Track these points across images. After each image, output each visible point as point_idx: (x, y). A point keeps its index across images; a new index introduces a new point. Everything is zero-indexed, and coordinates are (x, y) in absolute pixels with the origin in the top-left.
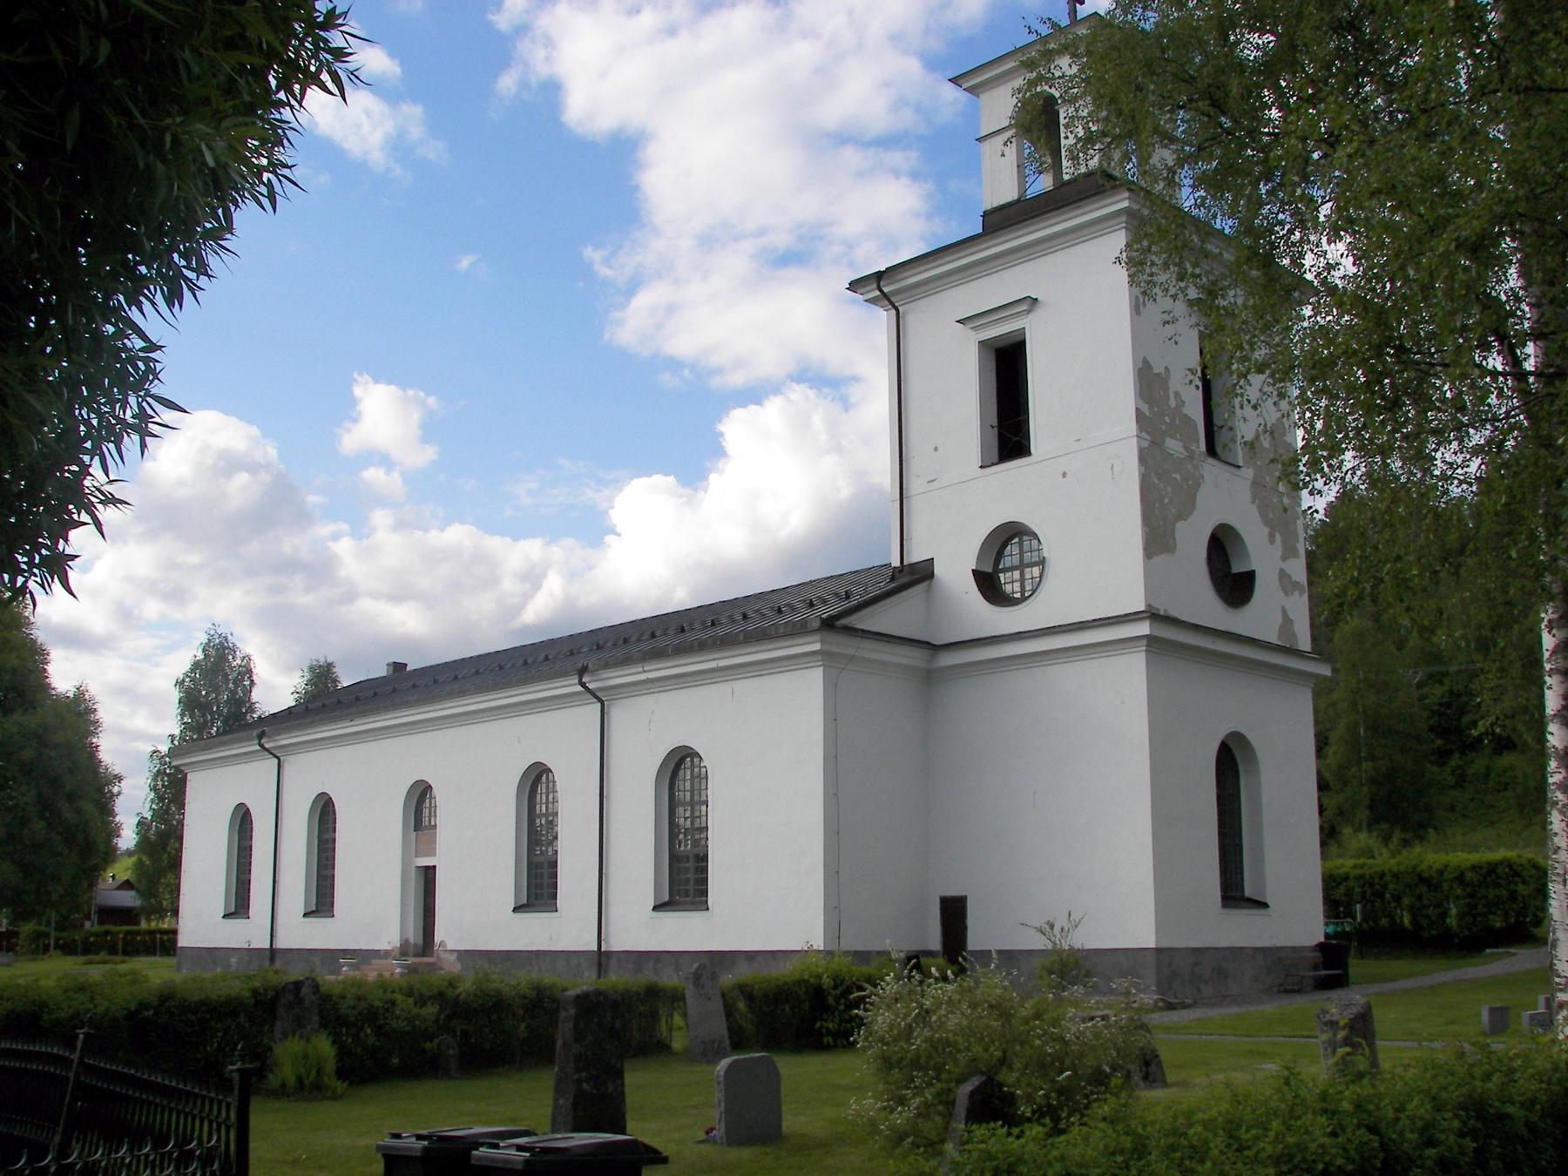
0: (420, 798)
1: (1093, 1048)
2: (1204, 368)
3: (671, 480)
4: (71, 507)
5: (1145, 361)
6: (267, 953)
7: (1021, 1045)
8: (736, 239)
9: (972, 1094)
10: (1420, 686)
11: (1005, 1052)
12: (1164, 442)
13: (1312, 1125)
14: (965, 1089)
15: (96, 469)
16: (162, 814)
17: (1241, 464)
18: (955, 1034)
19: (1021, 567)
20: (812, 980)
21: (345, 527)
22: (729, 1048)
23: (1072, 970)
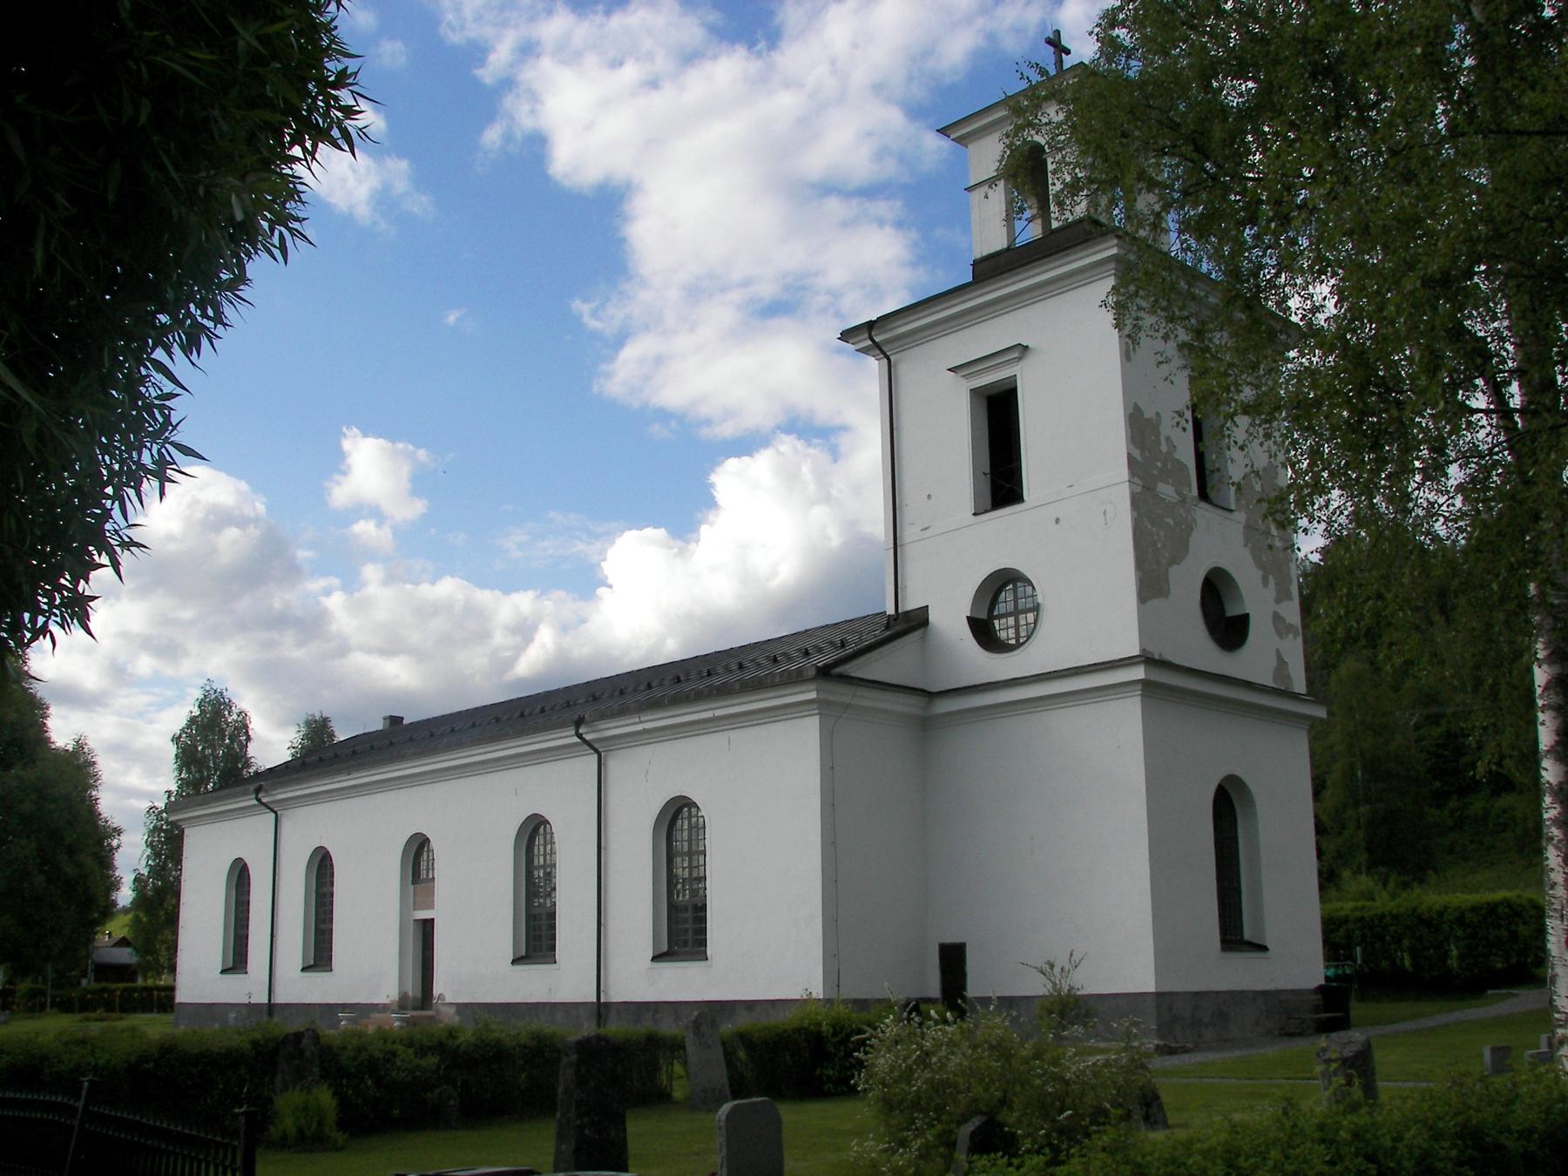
0: (418, 851)
1: (1093, 1087)
2: (1194, 408)
3: (661, 532)
4: (91, 548)
5: (1137, 408)
6: (266, 1008)
7: (1022, 1085)
8: (724, 289)
9: (973, 1134)
10: (1417, 727)
11: (1005, 1092)
12: (1156, 485)
13: (1309, 1154)
14: (968, 1128)
15: (116, 513)
16: (158, 871)
17: (1233, 508)
18: (956, 1075)
19: (1016, 613)
20: (812, 1027)
21: (335, 581)
22: (730, 1097)
23: (1072, 1010)
